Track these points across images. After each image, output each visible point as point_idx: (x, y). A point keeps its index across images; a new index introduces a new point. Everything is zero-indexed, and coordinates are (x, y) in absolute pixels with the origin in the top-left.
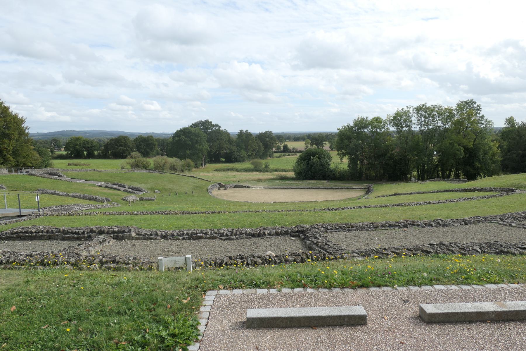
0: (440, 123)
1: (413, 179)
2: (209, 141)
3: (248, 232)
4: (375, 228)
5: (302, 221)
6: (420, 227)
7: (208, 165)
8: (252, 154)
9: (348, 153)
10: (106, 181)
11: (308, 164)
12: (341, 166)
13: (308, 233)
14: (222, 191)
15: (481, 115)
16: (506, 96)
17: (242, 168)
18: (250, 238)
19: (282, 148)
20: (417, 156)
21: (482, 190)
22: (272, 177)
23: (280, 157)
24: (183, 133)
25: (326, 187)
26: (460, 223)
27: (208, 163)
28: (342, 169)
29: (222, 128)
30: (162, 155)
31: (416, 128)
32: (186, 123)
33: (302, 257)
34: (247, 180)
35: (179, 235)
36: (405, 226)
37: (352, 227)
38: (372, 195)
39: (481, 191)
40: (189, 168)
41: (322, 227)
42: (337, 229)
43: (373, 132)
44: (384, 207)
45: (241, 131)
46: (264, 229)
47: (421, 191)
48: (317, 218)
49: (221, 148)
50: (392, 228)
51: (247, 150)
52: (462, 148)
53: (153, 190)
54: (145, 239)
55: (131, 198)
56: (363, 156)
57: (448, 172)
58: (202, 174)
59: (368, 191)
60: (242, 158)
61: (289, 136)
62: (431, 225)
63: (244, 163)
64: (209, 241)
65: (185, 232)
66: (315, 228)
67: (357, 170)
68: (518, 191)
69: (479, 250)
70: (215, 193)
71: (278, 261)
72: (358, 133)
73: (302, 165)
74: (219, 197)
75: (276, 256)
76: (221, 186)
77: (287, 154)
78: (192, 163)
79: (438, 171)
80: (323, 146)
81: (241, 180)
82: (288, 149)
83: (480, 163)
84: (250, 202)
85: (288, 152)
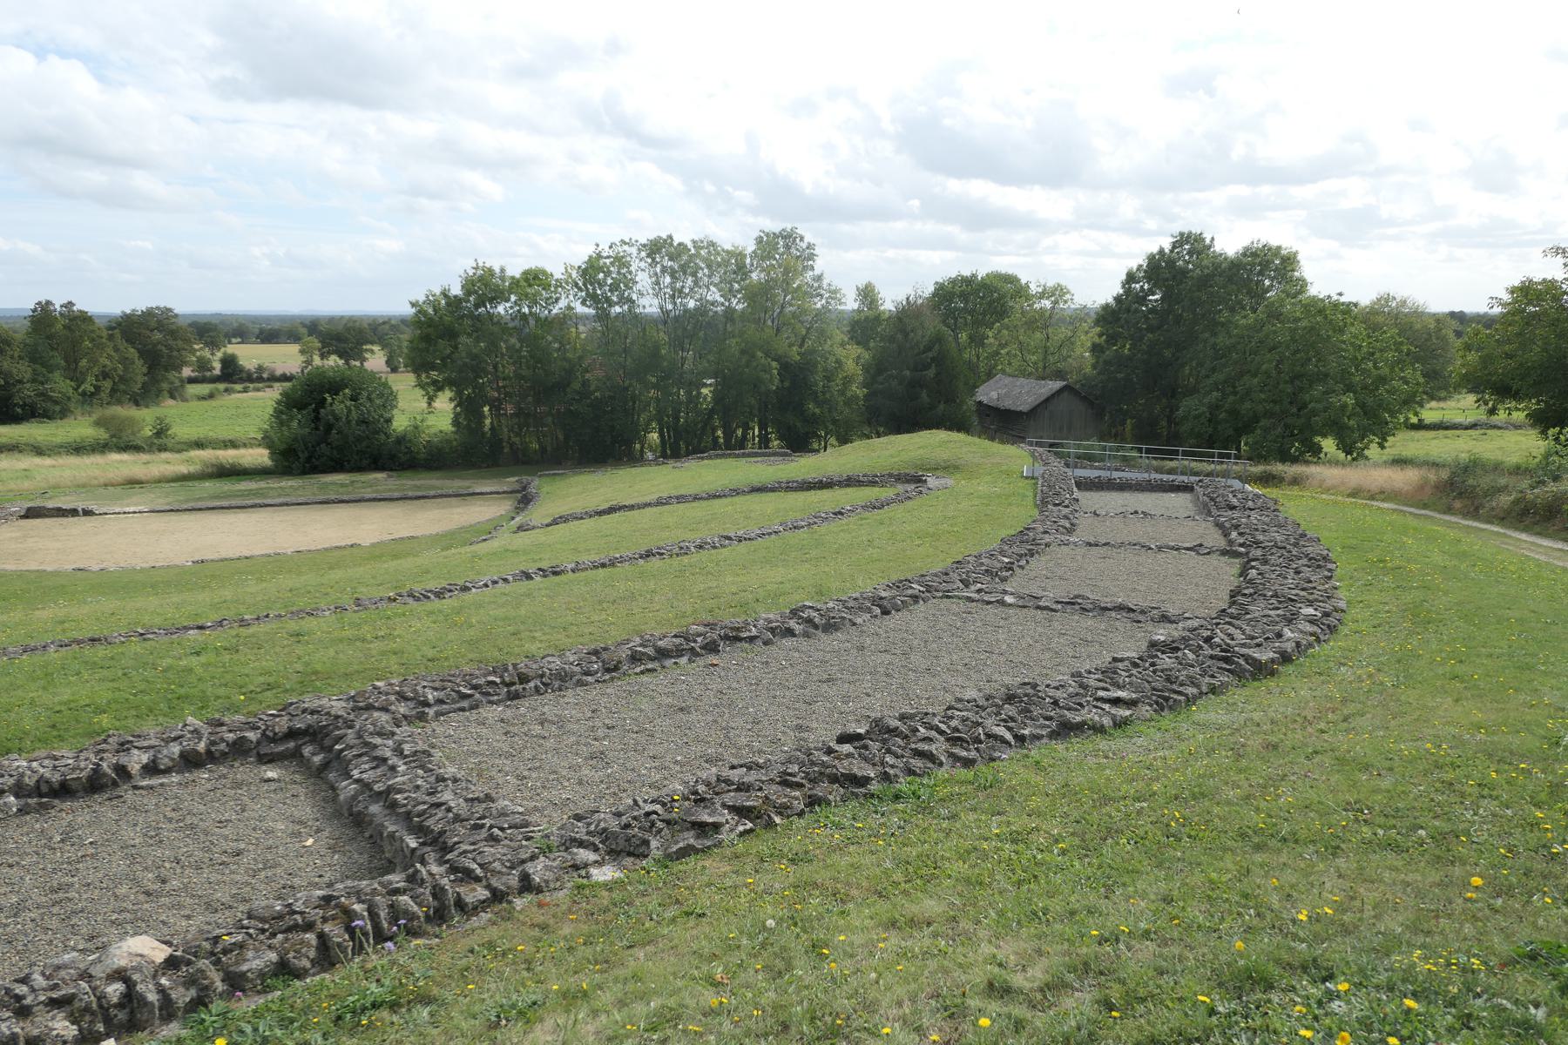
0: (714, 295)
1: (650, 456)
3: (29, 781)
4: (608, 670)
5: (310, 679)
8: (98, 388)
9: (450, 383)
11: (317, 419)
13: (339, 739)
15: (817, 272)
16: (845, 228)
17: (58, 440)
18: (43, 807)
19: (217, 366)
20: (655, 386)
21: (850, 482)
22: (184, 469)
23: (211, 396)
26: (869, 610)
28: (433, 431)
31: (649, 305)
33: (322, 936)
34: (82, 487)
36: (712, 648)
37: (524, 679)
38: (539, 513)
39: (848, 486)
41: (402, 697)
44: (603, 565)
46: (124, 747)
47: (682, 492)
48: (376, 646)
50: (669, 662)
51: (77, 378)
52: (774, 364)
56: (498, 389)
57: (739, 432)
59: (525, 500)
60: (56, 403)
61: (241, 325)
62: (790, 632)
63: (69, 421)
66: (370, 707)
67: (484, 434)
69: (1008, 736)
71: (182, 996)
73: (295, 424)
75: (171, 963)
77: (238, 387)
79: (714, 430)
81: (54, 487)
82: (241, 370)
83: (819, 404)
84: (96, 568)
85: (242, 381)
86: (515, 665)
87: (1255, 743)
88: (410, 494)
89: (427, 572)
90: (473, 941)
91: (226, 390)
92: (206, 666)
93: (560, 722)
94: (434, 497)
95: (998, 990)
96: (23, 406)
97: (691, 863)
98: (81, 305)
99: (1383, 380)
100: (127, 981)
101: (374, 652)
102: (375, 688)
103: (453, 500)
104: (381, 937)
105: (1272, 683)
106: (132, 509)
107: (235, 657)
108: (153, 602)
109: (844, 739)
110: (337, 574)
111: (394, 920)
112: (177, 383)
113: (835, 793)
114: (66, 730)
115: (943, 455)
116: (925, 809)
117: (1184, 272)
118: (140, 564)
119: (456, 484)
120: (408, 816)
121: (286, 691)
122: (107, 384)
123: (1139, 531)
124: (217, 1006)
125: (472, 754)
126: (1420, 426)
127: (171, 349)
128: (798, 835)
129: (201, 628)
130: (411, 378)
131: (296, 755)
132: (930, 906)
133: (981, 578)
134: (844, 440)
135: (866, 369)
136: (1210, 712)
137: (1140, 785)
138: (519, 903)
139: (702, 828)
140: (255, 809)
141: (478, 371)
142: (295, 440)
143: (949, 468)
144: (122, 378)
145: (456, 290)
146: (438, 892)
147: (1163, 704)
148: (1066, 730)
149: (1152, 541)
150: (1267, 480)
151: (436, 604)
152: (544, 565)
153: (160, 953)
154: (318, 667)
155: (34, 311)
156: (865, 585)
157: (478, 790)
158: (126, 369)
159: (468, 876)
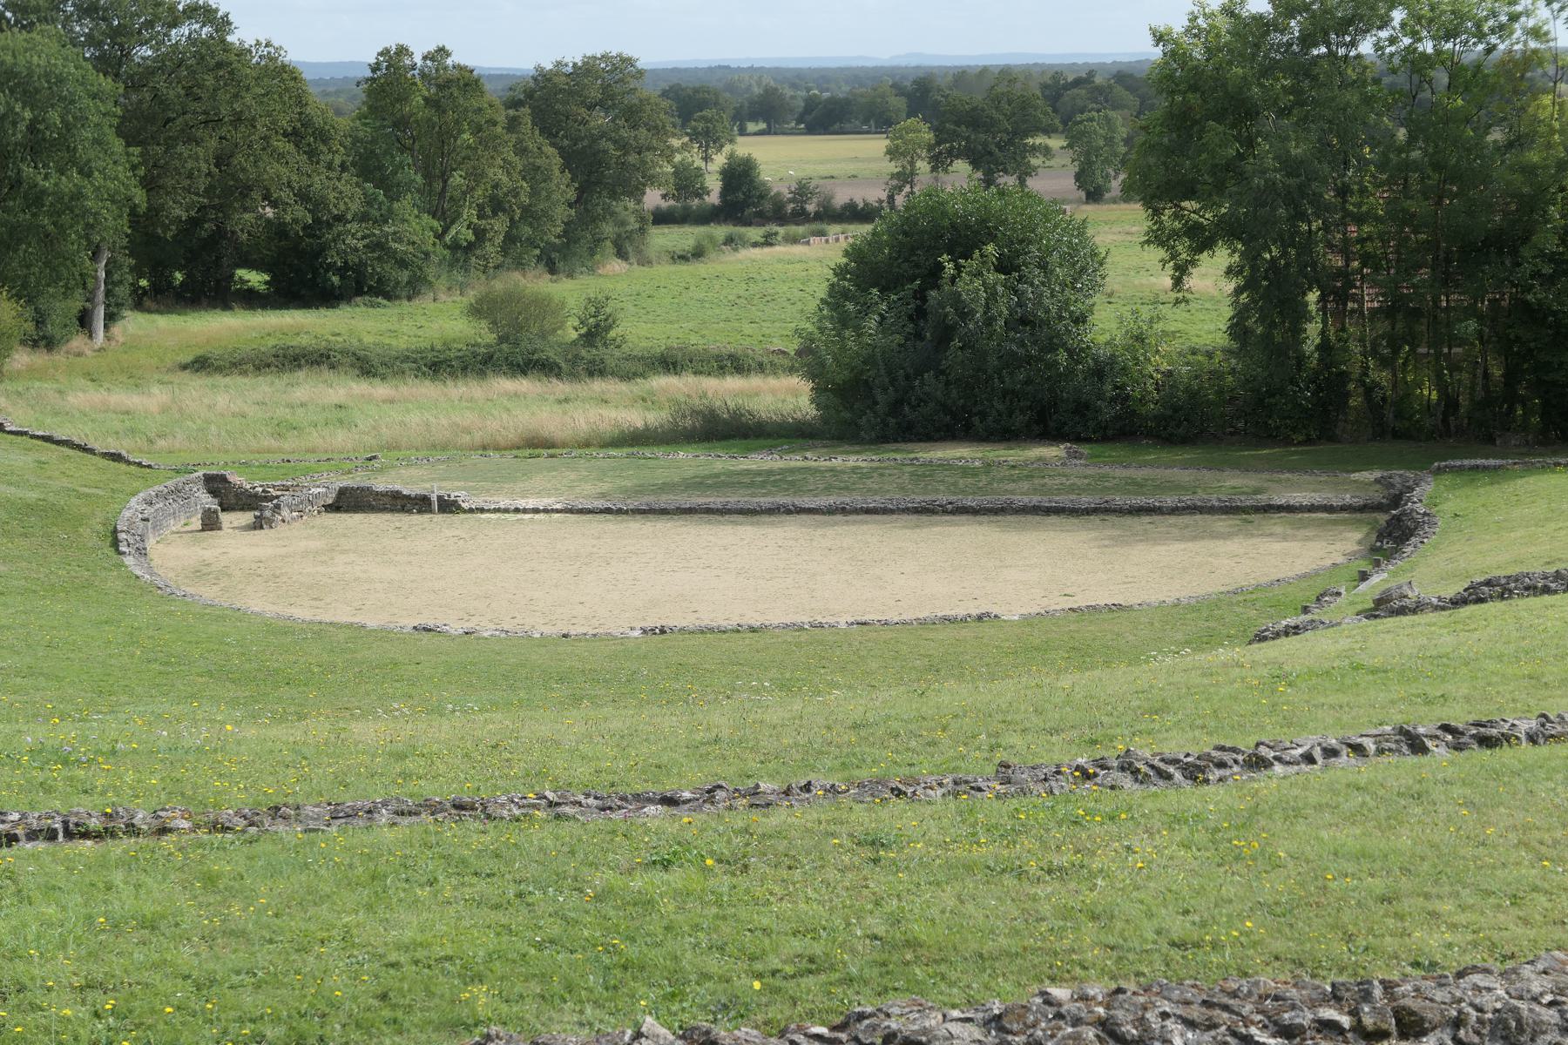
2: (142, 126)
7: (135, 324)
8: (480, 234)
9: (1229, 230)
11: (920, 314)
12: (1175, 320)
14: (235, 540)
17: (401, 344)
19: (714, 184)
22: (635, 418)
23: (698, 253)
25: (1064, 500)
27: (139, 306)
29: (243, 34)
34: (439, 449)
38: (1429, 569)
43: (1416, 64)
45: (394, 59)
48: (1049, 894)
49: (232, 188)
51: (444, 213)
58: (82, 397)
59: (1395, 530)
60: (402, 264)
63: (424, 303)
67: (1301, 360)
70: (177, 553)
72: (1305, 70)
73: (872, 323)
74: (208, 592)
76: (226, 495)
77: (755, 233)
80: (1025, 173)
81: (393, 446)
84: (456, 628)
85: (761, 219)
86: (1388, 986)
88: (1119, 500)
89: (1162, 709)
91: (729, 241)
92: (682, 895)
94: (1174, 511)
96: (342, 271)
98: (461, 56)
101: (1045, 909)
102: (1049, 1001)
103: (1222, 523)
106: (531, 503)
107: (742, 881)
108: (571, 725)
110: (951, 695)
112: (633, 224)
114: (409, 1009)
118: (542, 627)
119: (1232, 483)
121: (849, 980)
122: (499, 225)
127: (624, 147)
129: (670, 801)
130: (1135, 218)
141: (1298, 200)
142: (869, 360)
144: (526, 210)
151: (1184, 796)
152: (1459, 716)
154: (919, 930)
155: (375, 68)
158: (534, 193)
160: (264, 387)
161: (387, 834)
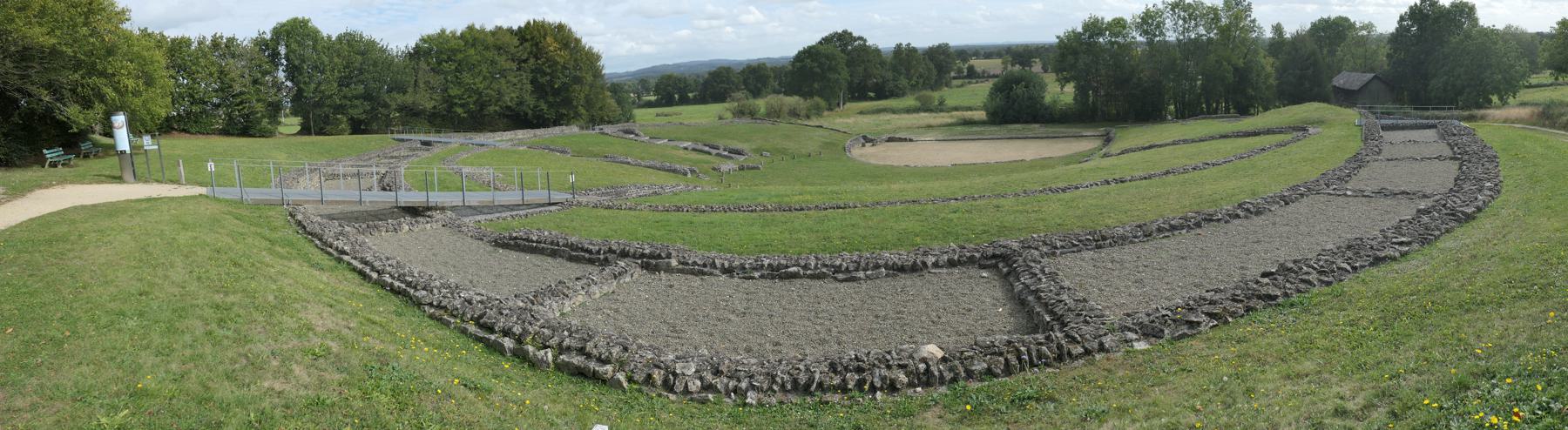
0: (1202, 30)
2: (851, 63)
5: (1003, 230)
6: (1222, 224)
7: (848, 105)
10: (695, 141)
12: (1062, 97)
14: (869, 149)
22: (950, 121)
24: (808, 54)
30: (779, 92)
31: (1171, 36)
32: (812, 38)
34: (908, 128)
35: (755, 269)
36: (1198, 225)
37: (1104, 238)
38: (1115, 148)
40: (818, 112)
41: (1045, 243)
42: (1076, 244)
43: (1112, 43)
46: (925, 253)
53: (759, 151)
54: (693, 273)
55: (727, 166)
58: (839, 120)
59: (1108, 140)
62: (1238, 216)
64: (811, 282)
65: (766, 262)
68: (1311, 130)
70: (857, 152)
71: (948, 376)
72: (1089, 44)
75: (944, 359)
76: (867, 140)
78: (823, 103)
87: (1466, 256)
90: (1075, 373)
93: (1122, 262)
95: (1340, 413)
97: (1185, 342)
99: (1512, 66)
100: (928, 366)
104: (1032, 365)
105: (1474, 223)
108: (937, 184)
109: (1264, 275)
110: (1015, 176)
111: (1040, 358)
113: (1260, 304)
115: (1316, 115)
116: (1306, 311)
117: (1427, 16)
120: (1046, 305)
123: (1412, 151)
124: (962, 383)
125: (1076, 275)
126: (1530, 86)
128: (1242, 328)
131: (995, 266)
132: (1308, 366)
133: (1333, 183)
134: (1266, 109)
135: (1277, 70)
136: (1447, 243)
137: (1412, 287)
138: (1098, 357)
139: (1191, 324)
140: (978, 290)
143: (1320, 122)
145: (1080, 30)
146: (1060, 347)
147: (1425, 241)
148: (1377, 261)
149: (1417, 157)
150: (1471, 118)
151: (1062, 195)
153: (940, 354)
156: (1277, 189)
157: (1080, 295)
159: (1073, 340)
160: (874, 117)
161: (899, 207)
